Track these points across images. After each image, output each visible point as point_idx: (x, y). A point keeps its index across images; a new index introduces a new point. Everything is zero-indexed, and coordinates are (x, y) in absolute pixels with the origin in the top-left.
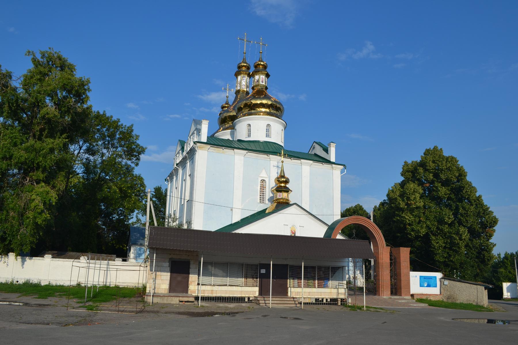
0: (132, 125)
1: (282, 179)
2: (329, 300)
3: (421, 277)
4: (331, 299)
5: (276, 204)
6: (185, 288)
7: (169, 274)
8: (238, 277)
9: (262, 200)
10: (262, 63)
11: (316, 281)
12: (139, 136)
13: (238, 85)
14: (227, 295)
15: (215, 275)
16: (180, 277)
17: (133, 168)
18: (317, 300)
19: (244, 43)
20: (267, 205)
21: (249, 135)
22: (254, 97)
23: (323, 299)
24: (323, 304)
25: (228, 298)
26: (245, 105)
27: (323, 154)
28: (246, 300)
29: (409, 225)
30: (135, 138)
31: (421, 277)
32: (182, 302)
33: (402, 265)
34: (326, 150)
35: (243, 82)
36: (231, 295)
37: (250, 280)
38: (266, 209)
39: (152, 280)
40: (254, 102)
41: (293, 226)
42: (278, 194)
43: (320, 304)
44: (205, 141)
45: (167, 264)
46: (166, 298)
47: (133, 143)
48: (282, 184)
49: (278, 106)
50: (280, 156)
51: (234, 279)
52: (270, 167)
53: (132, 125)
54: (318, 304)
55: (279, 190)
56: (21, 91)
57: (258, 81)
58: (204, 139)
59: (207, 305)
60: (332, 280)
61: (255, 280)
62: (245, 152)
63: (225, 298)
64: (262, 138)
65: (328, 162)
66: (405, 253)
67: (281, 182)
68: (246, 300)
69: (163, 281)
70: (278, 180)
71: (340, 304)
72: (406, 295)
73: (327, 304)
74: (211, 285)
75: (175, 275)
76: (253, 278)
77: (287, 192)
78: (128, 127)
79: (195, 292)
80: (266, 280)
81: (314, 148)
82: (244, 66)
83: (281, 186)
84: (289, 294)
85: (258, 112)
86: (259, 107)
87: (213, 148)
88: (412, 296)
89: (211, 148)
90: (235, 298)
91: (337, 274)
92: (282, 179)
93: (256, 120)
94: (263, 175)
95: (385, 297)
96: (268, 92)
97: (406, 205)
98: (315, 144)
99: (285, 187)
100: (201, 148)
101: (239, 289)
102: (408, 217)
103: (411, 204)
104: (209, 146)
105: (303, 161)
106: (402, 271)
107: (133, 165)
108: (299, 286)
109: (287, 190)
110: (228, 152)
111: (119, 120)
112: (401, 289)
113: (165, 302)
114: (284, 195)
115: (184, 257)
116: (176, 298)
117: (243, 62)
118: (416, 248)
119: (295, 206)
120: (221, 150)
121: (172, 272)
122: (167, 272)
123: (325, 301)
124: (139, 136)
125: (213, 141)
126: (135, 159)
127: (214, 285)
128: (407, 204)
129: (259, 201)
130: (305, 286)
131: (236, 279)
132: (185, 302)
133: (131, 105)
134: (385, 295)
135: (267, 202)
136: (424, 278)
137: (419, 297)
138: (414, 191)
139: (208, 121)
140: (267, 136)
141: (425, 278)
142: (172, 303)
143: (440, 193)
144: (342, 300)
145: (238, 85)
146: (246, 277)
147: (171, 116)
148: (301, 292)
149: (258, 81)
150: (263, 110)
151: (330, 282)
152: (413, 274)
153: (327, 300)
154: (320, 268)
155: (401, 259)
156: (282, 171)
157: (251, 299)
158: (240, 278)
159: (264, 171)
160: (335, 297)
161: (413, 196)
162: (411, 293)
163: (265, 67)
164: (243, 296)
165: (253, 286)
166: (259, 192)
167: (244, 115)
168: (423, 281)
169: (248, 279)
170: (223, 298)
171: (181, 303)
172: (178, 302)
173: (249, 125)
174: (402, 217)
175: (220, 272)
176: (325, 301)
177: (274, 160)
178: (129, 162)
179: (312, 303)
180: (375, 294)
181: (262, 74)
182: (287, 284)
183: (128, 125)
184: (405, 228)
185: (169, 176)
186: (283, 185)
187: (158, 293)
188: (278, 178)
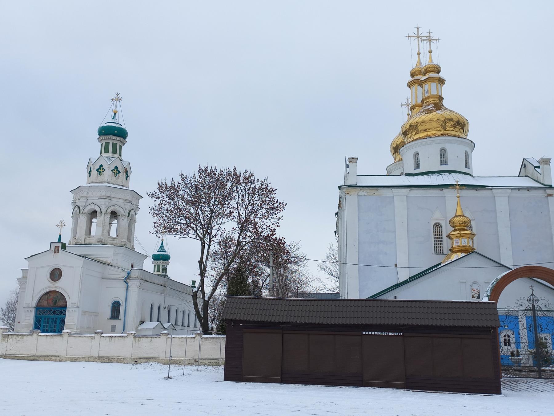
21: (417, 167)
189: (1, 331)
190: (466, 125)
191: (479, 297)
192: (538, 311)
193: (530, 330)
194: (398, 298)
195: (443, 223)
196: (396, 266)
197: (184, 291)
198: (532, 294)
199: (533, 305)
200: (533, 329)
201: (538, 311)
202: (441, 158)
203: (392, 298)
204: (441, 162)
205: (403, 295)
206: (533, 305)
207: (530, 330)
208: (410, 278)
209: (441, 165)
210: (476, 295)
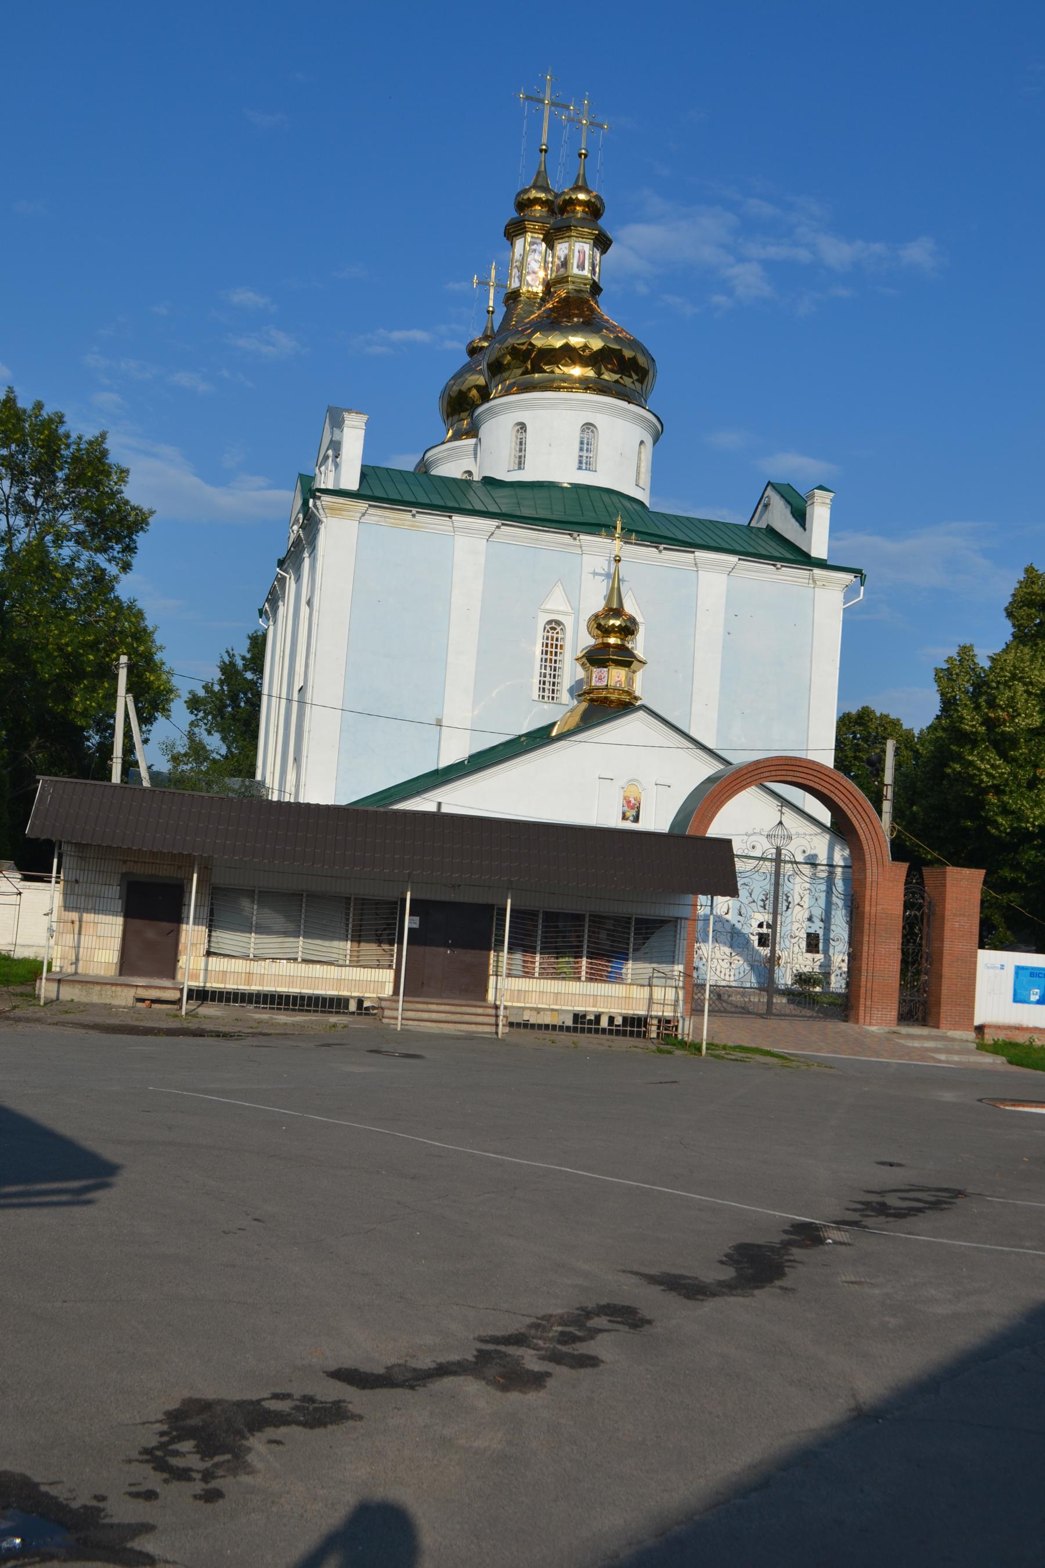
0: (103, 436)
1: (611, 622)
2: (619, 1021)
3: (1019, 969)
4: (625, 1019)
5: (585, 705)
6: (166, 963)
7: (120, 920)
8: (332, 938)
9: (548, 688)
10: (582, 196)
11: (584, 961)
12: (127, 471)
13: (515, 272)
14: (295, 990)
15: (261, 929)
16: (151, 931)
17: (116, 578)
18: (578, 1017)
19: (541, 112)
20: (563, 708)
21: (520, 464)
22: (553, 322)
23: (598, 1017)
24: (597, 1031)
25: (295, 998)
26: (512, 361)
27: (787, 527)
28: (353, 1006)
29: (998, 791)
30: (114, 477)
31: (1019, 969)
32: (142, 1000)
33: (948, 925)
34: (801, 516)
35: (534, 266)
36: (307, 991)
37: (370, 949)
38: (553, 724)
40: (539, 340)
41: (633, 782)
42: (596, 671)
43: (590, 1031)
45: (114, 892)
46: (98, 988)
47: (113, 495)
48: (613, 641)
49: (628, 354)
50: (611, 535)
51: (319, 942)
52: (579, 573)
53: (103, 436)
54: (583, 1030)
55: (595, 658)
57: (565, 264)
58: (351, 481)
59: (219, 1013)
60: (635, 960)
61: (386, 947)
62: (491, 524)
63: (288, 997)
64: (566, 473)
65: (803, 559)
66: (963, 889)
67: (607, 631)
68: (353, 1006)
69: (103, 939)
70: (599, 626)
71: (654, 1035)
72: (956, 1026)
73: (611, 1032)
74: (246, 957)
75: (138, 923)
76: (380, 942)
77: (627, 664)
78: (90, 443)
79: (196, 977)
80: (166, 926)
81: (766, 506)
82: (537, 201)
83: (608, 645)
84: (491, 997)
85: (553, 380)
86: (556, 363)
87: (379, 512)
88: (980, 1029)
89: (371, 511)
90: (317, 998)
91: (654, 941)
92: (611, 622)
94: (557, 605)
95: (873, 1028)
96: (604, 308)
97: (982, 724)
98: (770, 492)
99: (622, 649)
100: (334, 510)
101: (332, 972)
102: (988, 765)
103: (998, 718)
104: (362, 505)
105: (701, 554)
106: (947, 945)
107: (112, 569)
108: (528, 974)
109: (626, 659)
110: (433, 525)
111: (60, 419)
112: (938, 1004)
113: (95, 999)
114: (616, 676)
115: (166, 872)
116: (126, 990)
117: (535, 186)
118: (1024, 871)
119: (641, 714)
120: (408, 516)
121: (129, 914)
122: (114, 913)
123: (604, 1023)
124: (127, 471)
125: (380, 488)
126: (118, 547)
127: (257, 958)
128: (987, 722)
129: (535, 694)
130: (543, 975)
131: (327, 943)
132: (154, 1001)
133: (245, 297)
134: (878, 1021)
135: (565, 697)
136: (1032, 975)
137: (1001, 1036)
138: (1014, 677)
139: (365, 418)
140: (584, 464)
142: (115, 1002)
143: (214, 755)
144: (665, 1023)
145: (515, 272)
146: (358, 938)
147: (397, 335)
148: (526, 990)
149: (565, 264)
150: (577, 371)
151: (630, 964)
152: (986, 958)
153: (611, 1019)
154: (598, 920)
155: (948, 906)
156: (615, 594)
157: (366, 1004)
158: (340, 939)
159: (558, 593)
160: (642, 1012)
161: (1008, 694)
162: (977, 1022)
163: (595, 210)
164: (345, 993)
165: (378, 967)
166: (538, 663)
167: (507, 392)
168: (1023, 985)
169: (364, 946)
170: (280, 996)
171: (140, 1005)
172: (130, 1002)
173: (522, 427)
174: (971, 763)
175: (277, 920)
176: (604, 1023)
177: (595, 552)
178: (101, 559)
179: (561, 1028)
180: (846, 1019)
181: (582, 236)
182: (487, 965)
183: (88, 437)
184: (982, 805)
185: (267, 600)
186: (612, 640)
187: (86, 975)
188: (596, 616)
189: (1043, 810)
190: (651, 373)
191: (636, 819)
192: (785, 862)
193: (764, 907)
194: (445, 809)
195: (568, 621)
196: (439, 724)
197: (336, 1042)
198: (781, 823)
199: (779, 850)
200: (770, 905)
201: (785, 862)
202: (581, 450)
203: (432, 807)
204: (580, 462)
205: (460, 799)
206: (779, 850)
207: (764, 907)
208: (472, 758)
209: (580, 468)
210: (631, 813)
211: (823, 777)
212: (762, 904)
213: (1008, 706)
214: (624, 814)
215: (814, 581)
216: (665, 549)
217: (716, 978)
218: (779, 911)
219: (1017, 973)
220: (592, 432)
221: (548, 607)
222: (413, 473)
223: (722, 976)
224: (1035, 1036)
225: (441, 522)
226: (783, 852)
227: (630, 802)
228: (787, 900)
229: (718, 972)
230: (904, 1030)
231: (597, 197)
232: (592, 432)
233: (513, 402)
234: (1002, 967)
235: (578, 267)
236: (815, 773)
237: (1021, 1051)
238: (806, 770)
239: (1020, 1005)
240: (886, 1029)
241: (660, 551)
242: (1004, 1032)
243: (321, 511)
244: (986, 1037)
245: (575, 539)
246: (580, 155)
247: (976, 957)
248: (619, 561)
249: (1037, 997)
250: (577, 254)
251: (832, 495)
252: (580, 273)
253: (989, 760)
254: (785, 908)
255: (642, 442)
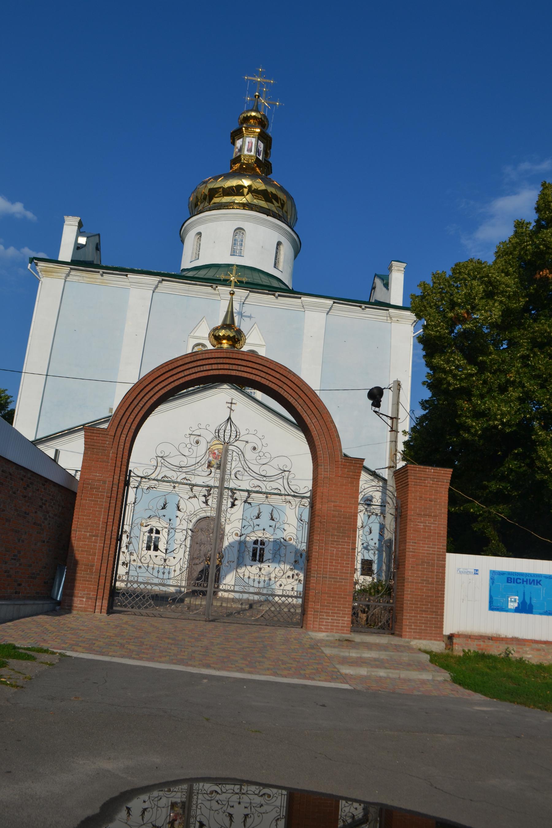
3: (493, 573)
31: (493, 573)
39: (295, 594)
44: (69, 260)
56: (427, 411)
62: (155, 280)
65: (387, 306)
72: (421, 635)
87: (78, 273)
89: (73, 273)
93: (212, 221)
120: (98, 276)
136: (509, 580)
137: (473, 647)
141: (513, 579)
152: (456, 562)
157: (300, 627)
162: (447, 631)
173: (200, 234)
193: (206, 502)
198: (229, 418)
202: (242, 241)
207: (206, 502)
211: (270, 371)
212: (204, 499)
213: (466, 303)
214: (210, 463)
215: (391, 318)
216: (279, 296)
217: (147, 574)
218: (224, 508)
219: (492, 580)
220: (243, 234)
221: (195, 335)
222: (88, 237)
223: (155, 574)
224: (511, 647)
225: (120, 279)
226: (231, 447)
227: (215, 453)
228: (232, 497)
229: (150, 569)
230: (358, 638)
231: (264, 115)
232: (243, 234)
233: (195, 221)
234: (476, 572)
235: (248, 150)
236: (261, 368)
237: (483, 669)
238: (250, 364)
239: (497, 613)
240: (337, 636)
241: (277, 298)
242: (476, 642)
243: (40, 274)
244: (456, 647)
245: (215, 289)
246: (255, 96)
247: (444, 560)
248: (233, 294)
249: (516, 605)
250: (247, 143)
251: (405, 265)
252: (249, 153)
253: (454, 362)
254: (230, 505)
255: (279, 244)
